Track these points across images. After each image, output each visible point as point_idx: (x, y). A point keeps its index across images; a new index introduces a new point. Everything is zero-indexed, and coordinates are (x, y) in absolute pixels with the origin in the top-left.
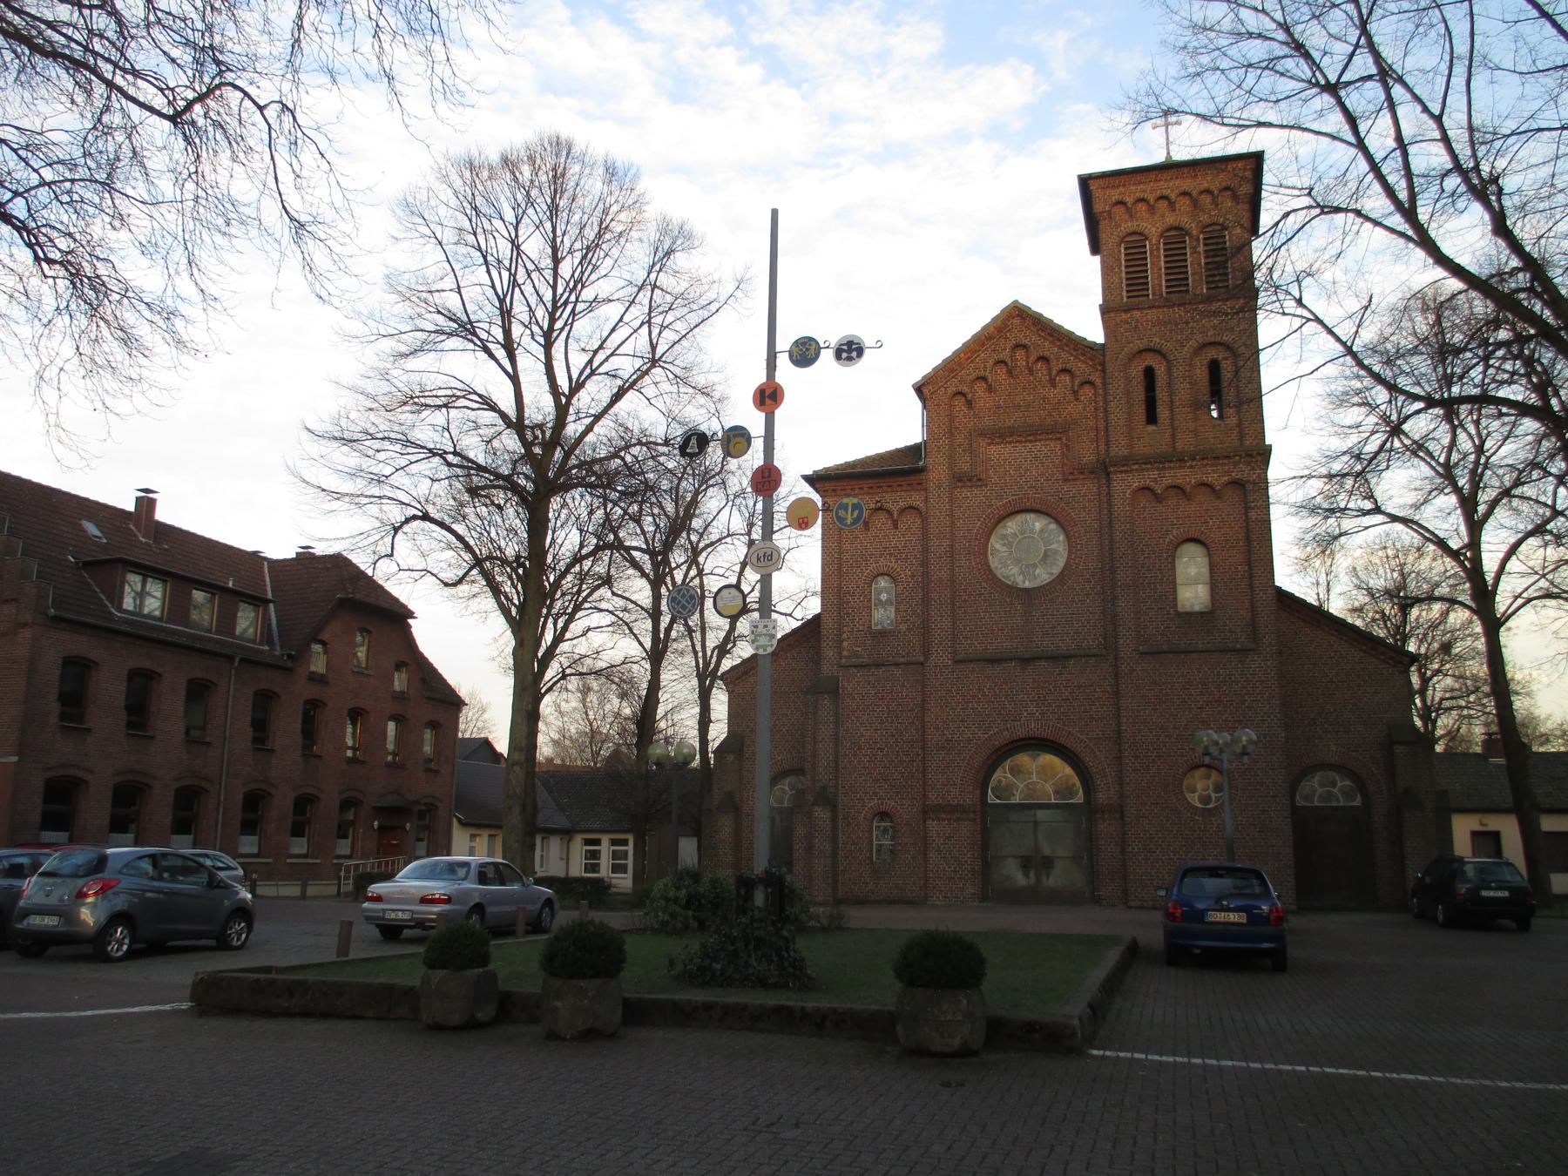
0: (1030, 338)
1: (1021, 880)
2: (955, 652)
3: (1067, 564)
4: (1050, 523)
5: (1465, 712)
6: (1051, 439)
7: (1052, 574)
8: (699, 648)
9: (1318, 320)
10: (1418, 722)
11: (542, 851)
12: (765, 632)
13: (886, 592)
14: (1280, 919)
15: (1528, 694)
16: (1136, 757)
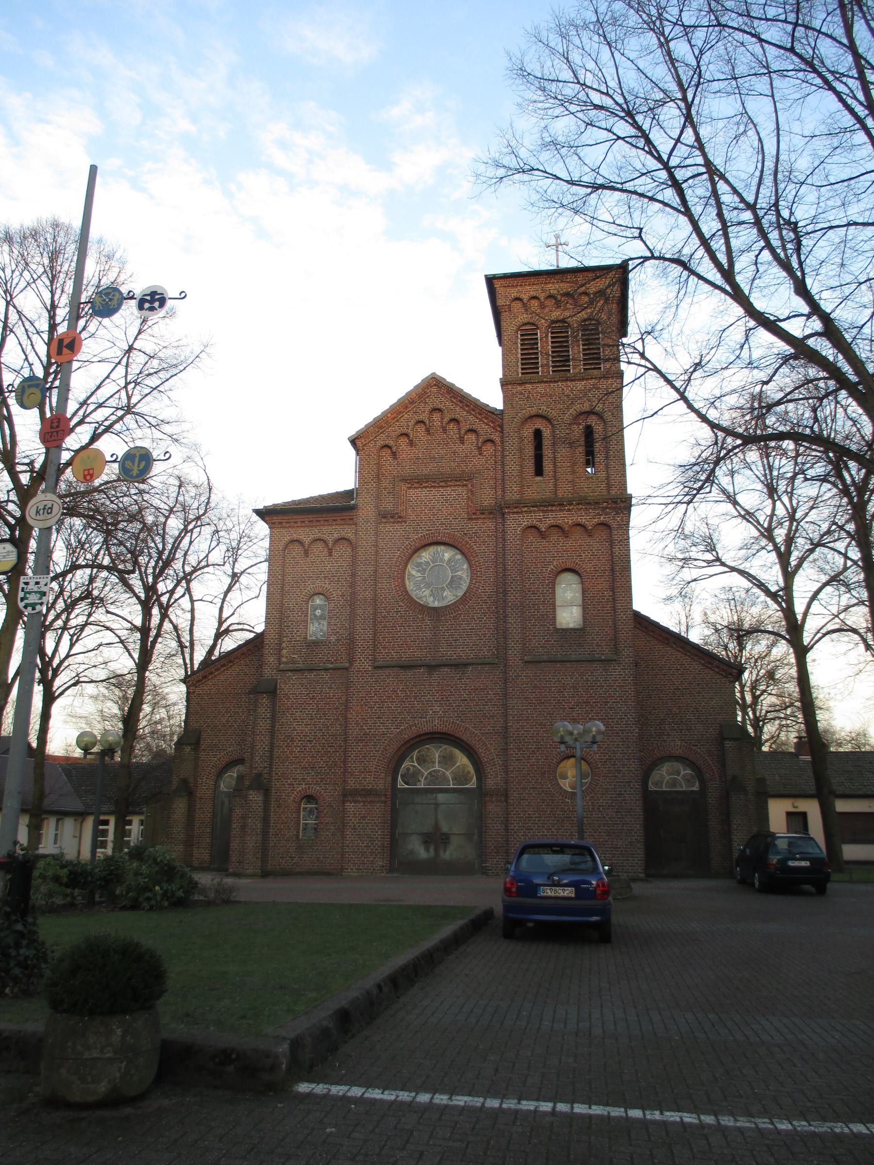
0: (445, 403)
1: (422, 853)
2: (374, 660)
3: (469, 588)
4: (456, 554)
5: (784, 722)
6: (459, 485)
8: (188, 661)
9: (656, 369)
10: (750, 729)
11: (57, 830)
12: (35, 589)
13: (321, 609)
14: (606, 893)
15: (827, 709)
16: (519, 749)
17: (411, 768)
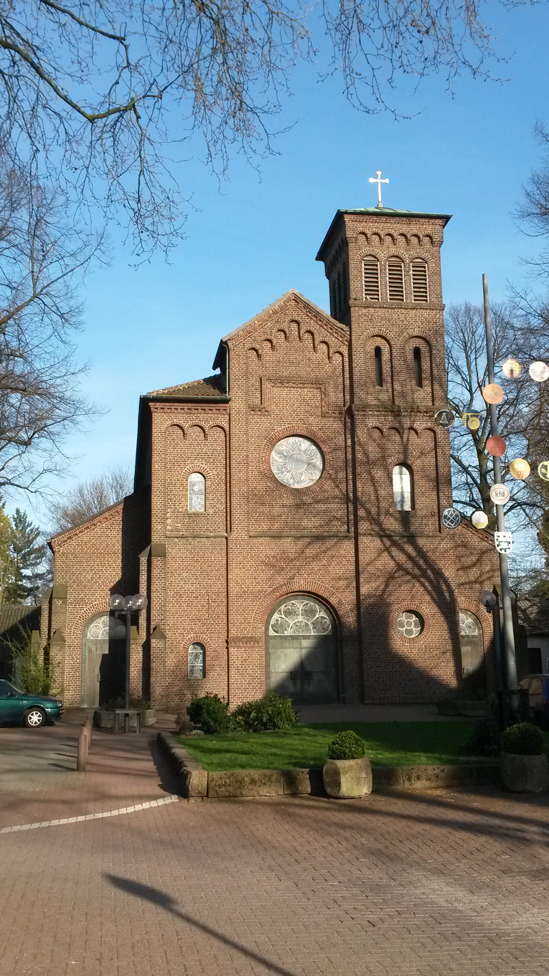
7: (312, 480)
17: (280, 619)
